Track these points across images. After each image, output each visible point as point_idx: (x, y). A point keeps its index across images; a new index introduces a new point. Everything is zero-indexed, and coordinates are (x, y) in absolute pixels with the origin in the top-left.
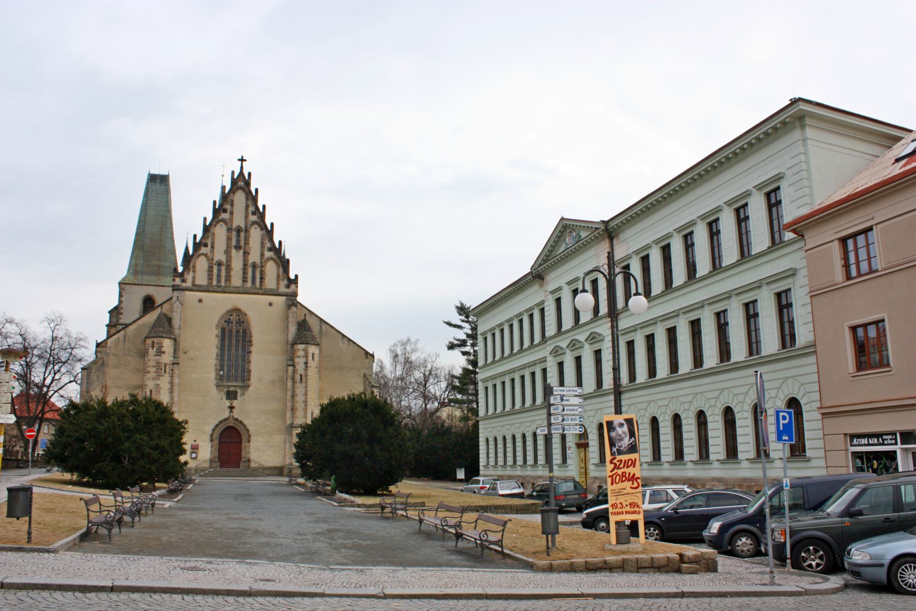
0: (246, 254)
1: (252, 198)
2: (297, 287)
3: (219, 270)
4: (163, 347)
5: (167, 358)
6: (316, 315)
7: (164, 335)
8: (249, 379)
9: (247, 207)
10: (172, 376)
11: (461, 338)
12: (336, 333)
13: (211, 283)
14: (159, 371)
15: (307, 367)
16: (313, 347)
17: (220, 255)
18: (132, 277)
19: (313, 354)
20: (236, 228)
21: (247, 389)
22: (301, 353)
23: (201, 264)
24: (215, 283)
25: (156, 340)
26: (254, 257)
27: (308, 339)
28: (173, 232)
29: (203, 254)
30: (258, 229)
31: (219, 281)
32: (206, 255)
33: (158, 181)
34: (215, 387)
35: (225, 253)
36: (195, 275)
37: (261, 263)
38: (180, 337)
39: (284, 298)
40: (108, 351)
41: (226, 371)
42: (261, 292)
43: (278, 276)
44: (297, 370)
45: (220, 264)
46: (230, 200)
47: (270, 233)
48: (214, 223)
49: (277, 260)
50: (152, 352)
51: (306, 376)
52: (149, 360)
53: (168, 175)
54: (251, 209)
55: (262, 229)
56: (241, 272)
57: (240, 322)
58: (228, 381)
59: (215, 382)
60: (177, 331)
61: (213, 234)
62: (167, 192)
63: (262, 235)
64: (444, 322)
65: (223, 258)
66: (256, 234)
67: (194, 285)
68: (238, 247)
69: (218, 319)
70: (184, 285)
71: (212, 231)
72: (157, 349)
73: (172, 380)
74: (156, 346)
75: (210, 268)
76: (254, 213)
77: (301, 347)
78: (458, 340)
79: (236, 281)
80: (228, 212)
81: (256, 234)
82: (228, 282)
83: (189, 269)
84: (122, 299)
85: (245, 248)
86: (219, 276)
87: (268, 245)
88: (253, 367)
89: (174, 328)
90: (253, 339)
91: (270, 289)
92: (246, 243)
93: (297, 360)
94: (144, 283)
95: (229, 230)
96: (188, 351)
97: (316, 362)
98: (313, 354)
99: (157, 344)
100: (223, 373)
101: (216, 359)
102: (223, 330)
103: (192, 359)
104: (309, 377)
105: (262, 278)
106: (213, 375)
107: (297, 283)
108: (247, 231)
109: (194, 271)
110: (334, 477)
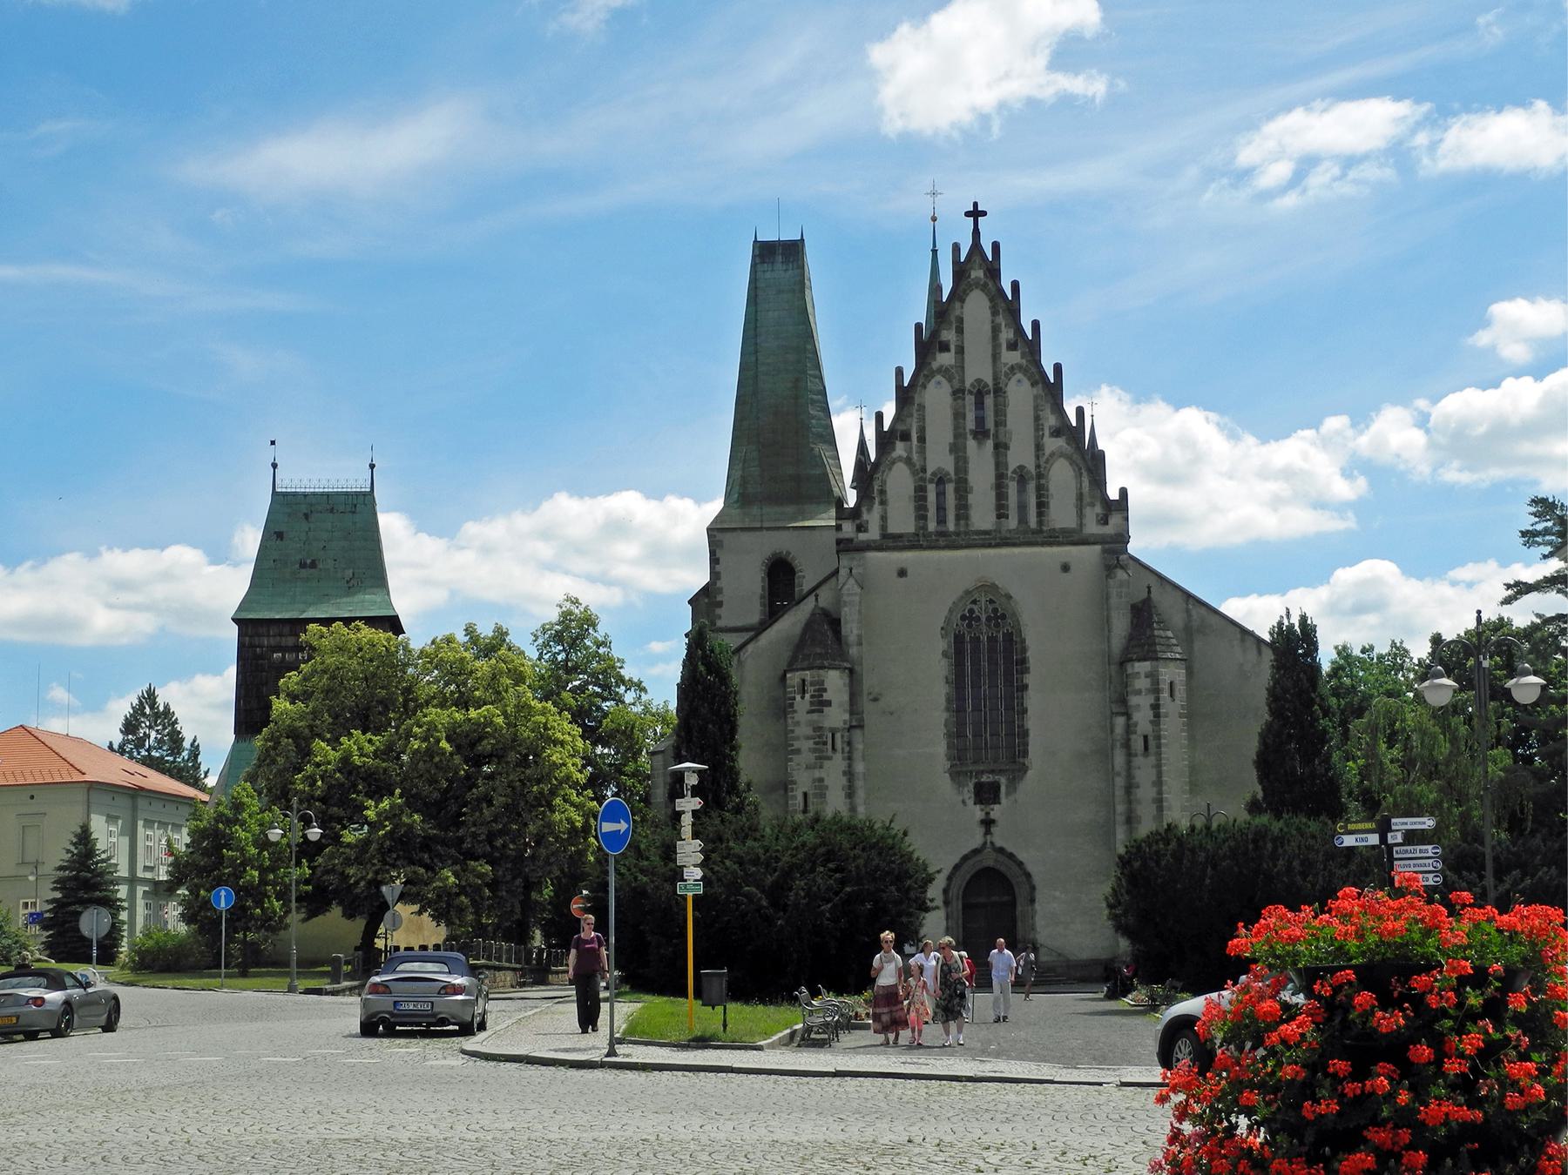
0: (1001, 448)
5: (836, 716)
9: (996, 330)
10: (850, 758)
13: (925, 528)
15: (1157, 716)
17: (939, 458)
19: (1171, 684)
20: (972, 385)
22: (1142, 683)
24: (932, 526)
25: (808, 675)
26: (1020, 455)
30: (1026, 383)
31: (942, 520)
33: (779, 258)
35: (951, 451)
37: (1038, 466)
39: (1098, 548)
44: (1136, 725)
45: (941, 481)
46: (953, 319)
48: (921, 380)
50: (802, 704)
51: (1158, 738)
53: (802, 240)
54: (1006, 335)
59: (948, 765)
61: (922, 407)
63: (1036, 397)
66: (1020, 394)
68: (980, 433)
70: (862, 537)
71: (917, 400)
72: (812, 696)
73: (850, 766)
74: (810, 689)
76: (1012, 346)
77: (1143, 667)
79: (982, 516)
80: (953, 348)
85: (996, 436)
86: (941, 508)
88: (1032, 723)
92: (1000, 422)
93: (1134, 700)
95: (958, 393)
97: (1178, 702)
101: (948, 709)
102: (959, 639)
104: (1163, 741)
105: (1042, 506)
106: (941, 748)
108: (999, 391)
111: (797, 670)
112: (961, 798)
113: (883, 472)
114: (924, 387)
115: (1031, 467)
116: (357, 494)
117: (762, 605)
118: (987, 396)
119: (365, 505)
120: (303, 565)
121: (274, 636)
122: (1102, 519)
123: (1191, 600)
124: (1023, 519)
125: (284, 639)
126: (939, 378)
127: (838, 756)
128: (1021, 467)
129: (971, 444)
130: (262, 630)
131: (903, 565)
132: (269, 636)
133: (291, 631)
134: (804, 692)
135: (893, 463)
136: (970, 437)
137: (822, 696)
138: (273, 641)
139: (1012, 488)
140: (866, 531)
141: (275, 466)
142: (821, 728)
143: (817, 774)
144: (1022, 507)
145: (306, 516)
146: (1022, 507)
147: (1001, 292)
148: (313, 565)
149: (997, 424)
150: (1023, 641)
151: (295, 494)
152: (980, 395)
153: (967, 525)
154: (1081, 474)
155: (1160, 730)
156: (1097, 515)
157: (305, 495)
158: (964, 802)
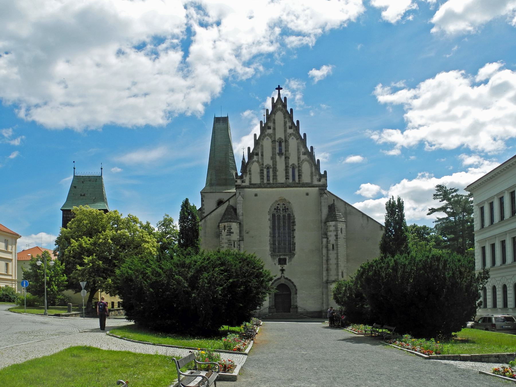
0: (287, 158)
5: (235, 237)
9: (285, 123)
13: (263, 182)
15: (337, 238)
17: (268, 161)
22: (332, 228)
24: (265, 181)
25: (226, 224)
26: (293, 160)
30: (295, 139)
31: (268, 180)
32: (258, 162)
35: (271, 159)
37: (299, 164)
39: (317, 188)
47: (303, 141)
51: (337, 245)
53: (228, 117)
54: (289, 124)
60: (241, 218)
61: (262, 146)
63: (298, 143)
66: (293, 143)
67: (251, 184)
68: (281, 154)
70: (244, 184)
71: (261, 143)
72: (227, 231)
74: (227, 229)
79: (281, 179)
80: (272, 128)
82: (275, 180)
86: (268, 176)
92: (287, 150)
93: (329, 234)
94: (217, 191)
95: (274, 142)
98: (341, 229)
101: (270, 236)
102: (274, 215)
105: (300, 176)
108: (286, 141)
109: (250, 174)
113: (250, 165)
114: (263, 140)
115: (296, 164)
120: (81, 195)
124: (294, 179)
126: (267, 137)
128: (293, 164)
129: (278, 157)
134: (225, 229)
136: (277, 155)
139: (290, 171)
140: (245, 182)
142: (230, 240)
145: (83, 182)
148: (84, 195)
150: (294, 216)
154: (312, 166)
156: (317, 179)
157: (83, 176)
158: (275, 264)
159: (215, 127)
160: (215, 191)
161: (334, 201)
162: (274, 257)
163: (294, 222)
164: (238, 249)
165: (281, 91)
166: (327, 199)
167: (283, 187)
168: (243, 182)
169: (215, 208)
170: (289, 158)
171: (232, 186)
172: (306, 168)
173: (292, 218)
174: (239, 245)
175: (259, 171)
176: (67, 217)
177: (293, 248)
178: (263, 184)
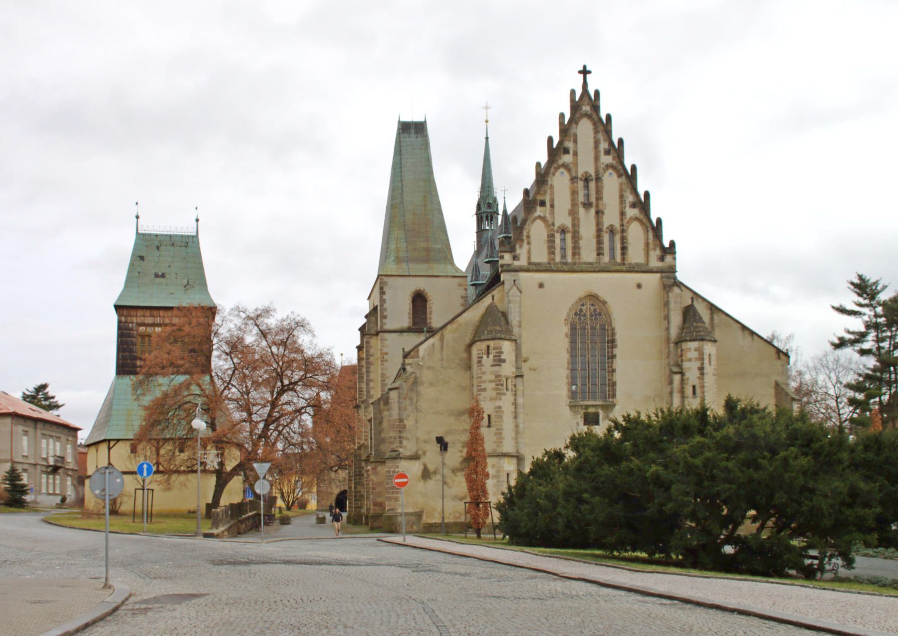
0: (599, 213)
1: (604, 126)
2: (675, 259)
3: (563, 240)
4: (502, 353)
5: (508, 369)
6: (704, 300)
7: (503, 336)
8: (614, 396)
9: (597, 143)
10: (515, 395)
11: (856, 330)
12: (732, 321)
13: (554, 259)
14: (500, 387)
15: (702, 374)
16: (710, 344)
17: (562, 218)
18: (395, 266)
19: (710, 355)
20: (582, 175)
21: (612, 410)
22: (693, 354)
23: (537, 231)
24: (558, 259)
25: (492, 344)
26: (611, 218)
27: (702, 333)
28: (439, 202)
29: (540, 217)
30: (615, 175)
31: (564, 256)
32: (543, 219)
33: (413, 131)
34: (568, 408)
35: (569, 214)
36: (530, 249)
37: (622, 225)
38: (520, 338)
39: (658, 275)
40: (421, 363)
41: (579, 385)
42: (624, 268)
43: (647, 244)
44: (688, 379)
45: (563, 231)
46: (572, 135)
47: (631, 178)
48: (552, 170)
49: (644, 220)
50: (488, 361)
51: (703, 387)
52: (484, 373)
53: (425, 121)
54: (604, 146)
55: (620, 176)
56: (594, 241)
57: (596, 315)
58: (583, 399)
59: (568, 401)
60: (516, 331)
61: (552, 187)
62: (426, 145)
63: (621, 184)
64: (833, 308)
65: (568, 222)
66: (611, 183)
67: (530, 263)
68: (587, 205)
69: (567, 310)
70: (516, 263)
71: (550, 183)
72: (495, 356)
73: (515, 399)
74: (493, 353)
75: (551, 237)
76: (607, 153)
77: (694, 345)
78: (853, 333)
79: (588, 255)
80: (571, 152)
81: (611, 183)
82: (577, 257)
83: (522, 240)
84: (384, 297)
85: (597, 206)
86: (563, 249)
87: (630, 198)
88: (618, 377)
89: (512, 327)
90: (617, 337)
91: (637, 264)
92: (599, 198)
93: (686, 365)
94: (411, 274)
95: (574, 179)
96: (528, 358)
97: (712, 366)
98: (710, 355)
99: (494, 349)
100: (576, 388)
101: (568, 368)
102: (573, 328)
103: (535, 370)
104: (706, 389)
105: (624, 249)
106: (564, 392)
107: (674, 253)
108: (598, 179)
109: (529, 243)
110: (828, 538)
111: (485, 340)
112: (576, 421)
113: (529, 224)
114: (554, 175)
115: (617, 226)
116: (188, 236)
117: (409, 318)
118: (591, 180)
119: (193, 242)
120: (157, 276)
121: (140, 316)
122: (660, 258)
123: (713, 308)
124: (613, 256)
125: (146, 318)
126: (562, 170)
127: (509, 393)
128: (612, 226)
129: (581, 210)
130: (133, 312)
131: (541, 281)
132: (137, 316)
133: (150, 313)
134: (488, 353)
135: (534, 220)
136: (581, 206)
137: (500, 356)
138: (140, 320)
139: (606, 238)
140: (518, 259)
141: (137, 217)
142: (500, 376)
143: (498, 403)
144: (612, 249)
145: (158, 248)
146: (612, 249)
147: (600, 119)
148: (163, 276)
149: (597, 199)
150: (613, 329)
151: (150, 235)
152: (587, 180)
153: (579, 258)
154: (648, 231)
155: (703, 383)
156: (657, 256)
157: (157, 236)
158: (578, 424)
159: (400, 142)
160: (408, 274)
161: (692, 301)
162: (577, 409)
163: (613, 341)
164: (514, 393)
165: (588, 76)
166: (681, 297)
167: (594, 271)
168: (515, 258)
169: (460, 309)
170: (603, 213)
171: (440, 263)
172: (636, 234)
173: (609, 332)
174: (515, 386)
175: (545, 238)
176: (128, 323)
177: (610, 393)
178: (554, 264)
